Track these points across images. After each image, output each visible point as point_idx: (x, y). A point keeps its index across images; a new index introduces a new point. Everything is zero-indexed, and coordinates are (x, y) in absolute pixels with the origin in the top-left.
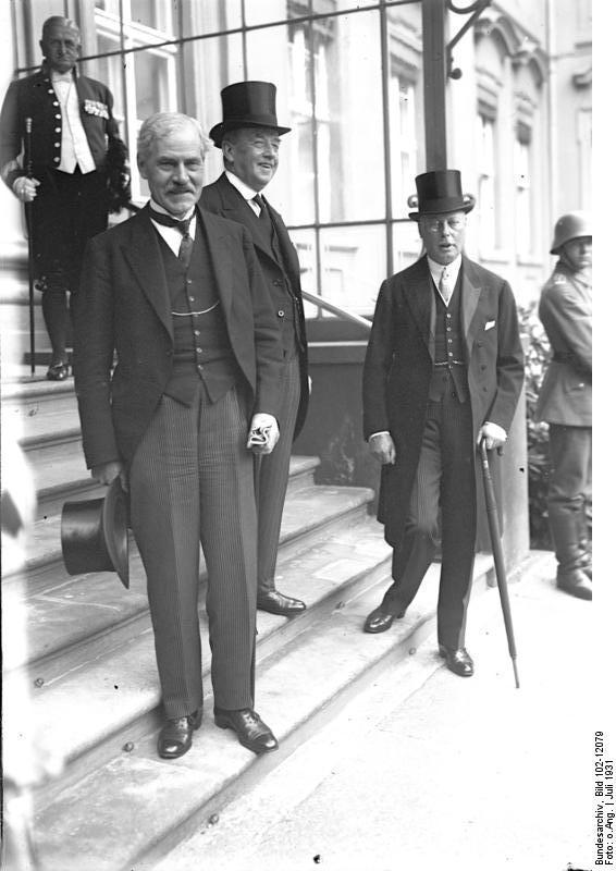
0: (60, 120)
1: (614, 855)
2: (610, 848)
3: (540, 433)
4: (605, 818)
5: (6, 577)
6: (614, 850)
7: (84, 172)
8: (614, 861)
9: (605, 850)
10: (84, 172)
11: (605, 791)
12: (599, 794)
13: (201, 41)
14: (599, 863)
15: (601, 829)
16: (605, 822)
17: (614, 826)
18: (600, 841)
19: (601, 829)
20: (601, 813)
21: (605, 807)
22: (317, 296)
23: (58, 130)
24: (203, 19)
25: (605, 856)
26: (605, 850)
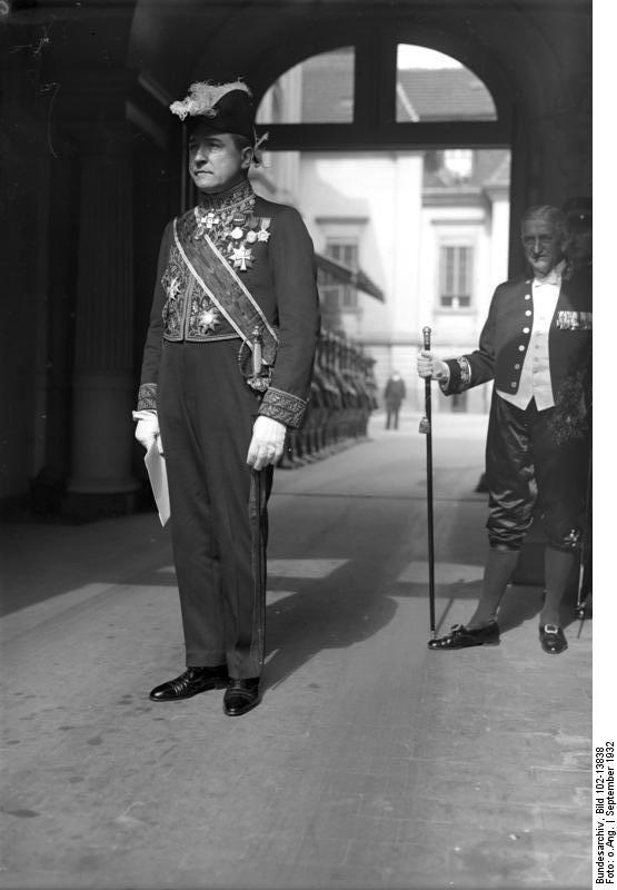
0: (531, 318)
1: (615, 873)
2: (611, 866)
3: (570, 731)
4: (606, 836)
5: (545, 368)
6: (615, 869)
7: (540, 408)
8: (615, 880)
9: (606, 868)
10: (540, 408)
11: (606, 809)
12: (600, 811)
13: (435, 503)
14: (599, 881)
15: (601, 847)
16: (606, 840)
17: (615, 844)
18: (601, 859)
19: (601, 847)
20: (602, 830)
21: (605, 824)
22: (447, 384)
23: (528, 313)
24: (456, 290)
25: (606, 874)
26: (606, 868)
